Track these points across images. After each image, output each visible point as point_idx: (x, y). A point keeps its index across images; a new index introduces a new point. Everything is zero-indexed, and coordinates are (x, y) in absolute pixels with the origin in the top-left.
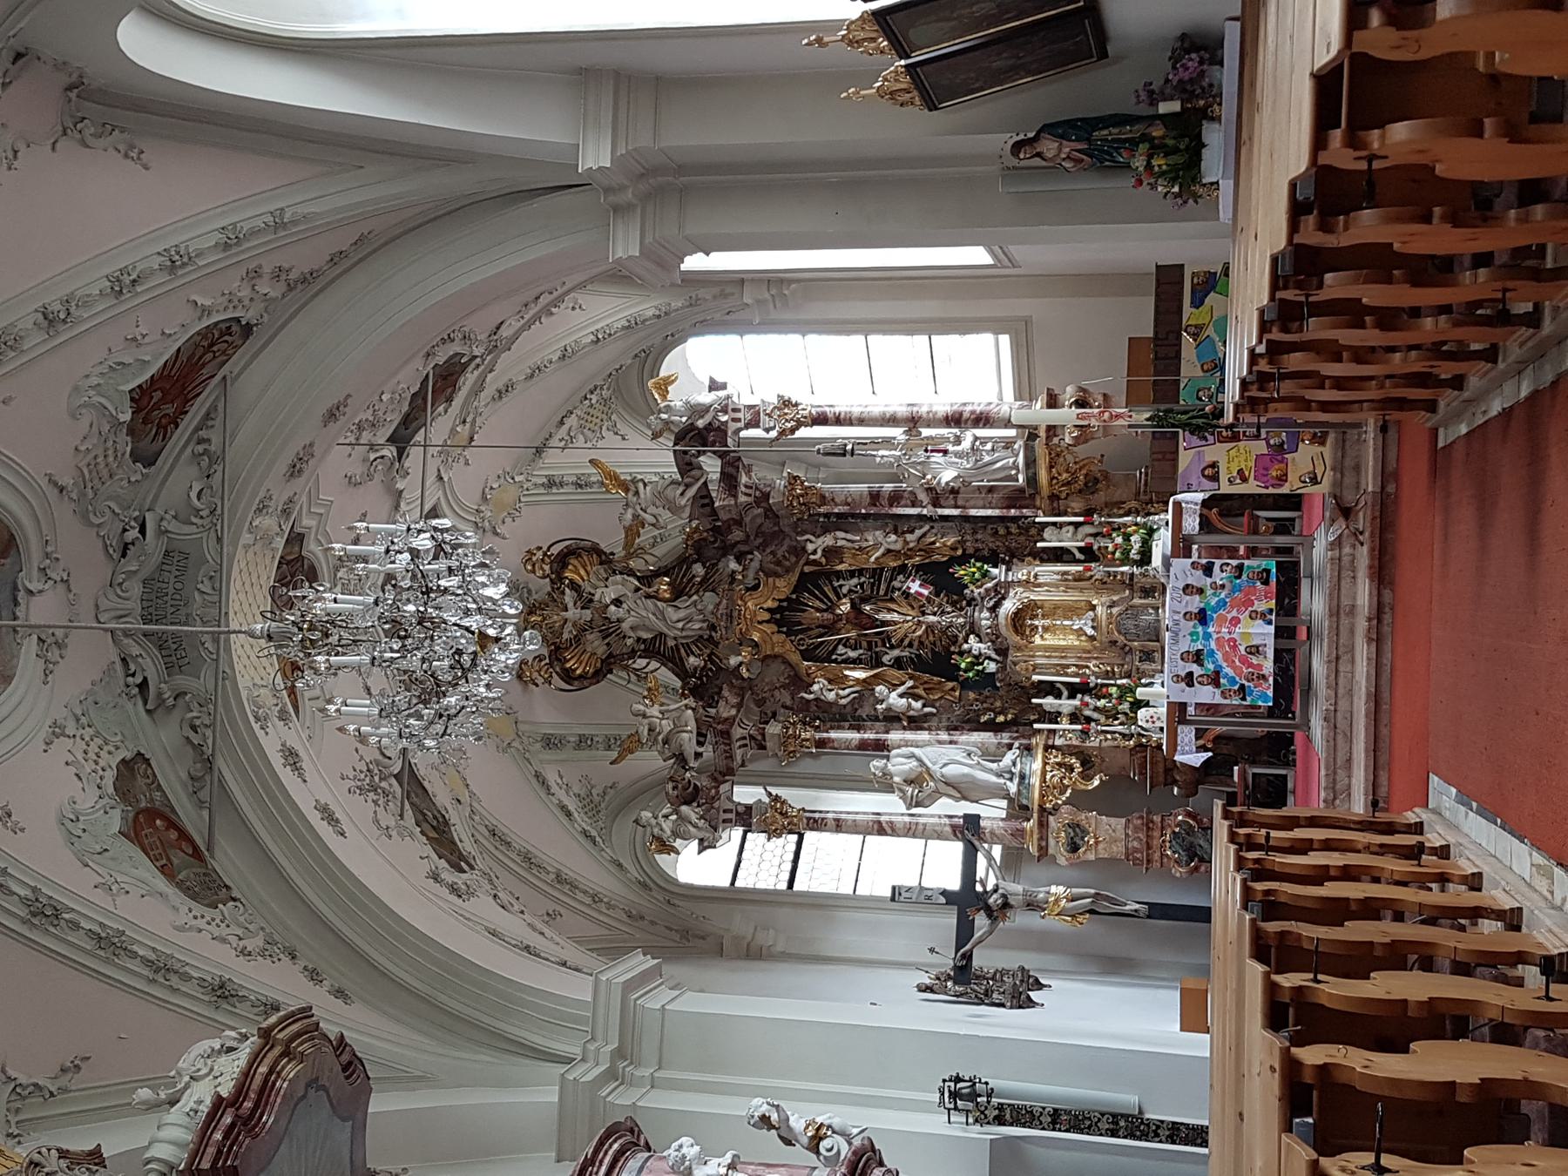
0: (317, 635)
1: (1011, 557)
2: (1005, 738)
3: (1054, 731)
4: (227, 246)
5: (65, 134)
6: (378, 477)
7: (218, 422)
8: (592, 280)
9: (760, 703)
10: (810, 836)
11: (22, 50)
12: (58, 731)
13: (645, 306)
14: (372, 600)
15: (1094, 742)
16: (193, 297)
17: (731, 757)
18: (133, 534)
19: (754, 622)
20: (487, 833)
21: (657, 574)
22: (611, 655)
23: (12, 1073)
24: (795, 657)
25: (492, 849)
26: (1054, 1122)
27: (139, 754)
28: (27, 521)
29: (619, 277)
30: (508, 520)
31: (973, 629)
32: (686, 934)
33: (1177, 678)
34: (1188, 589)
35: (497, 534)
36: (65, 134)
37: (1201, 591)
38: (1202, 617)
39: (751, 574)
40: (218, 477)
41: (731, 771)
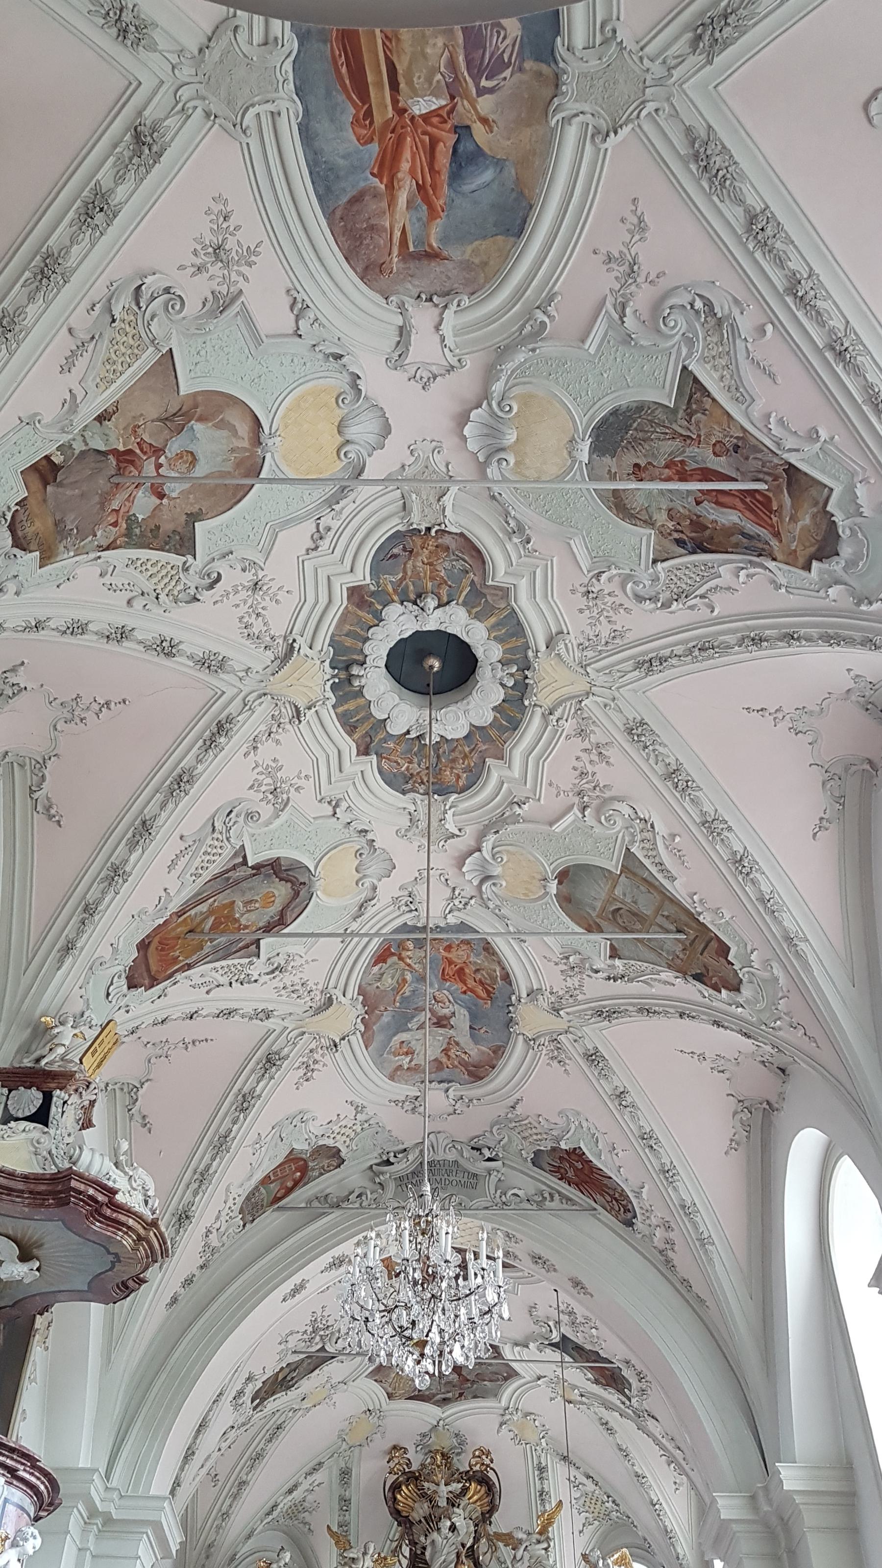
0: (423, 1225)
4: (683, 1207)
5: (739, 1101)
6: (536, 1328)
7: (565, 1206)
11: (787, 1073)
12: (359, 1109)
14: (448, 1258)
16: (646, 1186)
18: (487, 1154)
20: (279, 1422)
22: (412, 1524)
23: (146, 1084)
25: (267, 1428)
27: (344, 1161)
29: (703, 1509)
30: (511, 1435)
35: (501, 1426)
36: (739, 1101)
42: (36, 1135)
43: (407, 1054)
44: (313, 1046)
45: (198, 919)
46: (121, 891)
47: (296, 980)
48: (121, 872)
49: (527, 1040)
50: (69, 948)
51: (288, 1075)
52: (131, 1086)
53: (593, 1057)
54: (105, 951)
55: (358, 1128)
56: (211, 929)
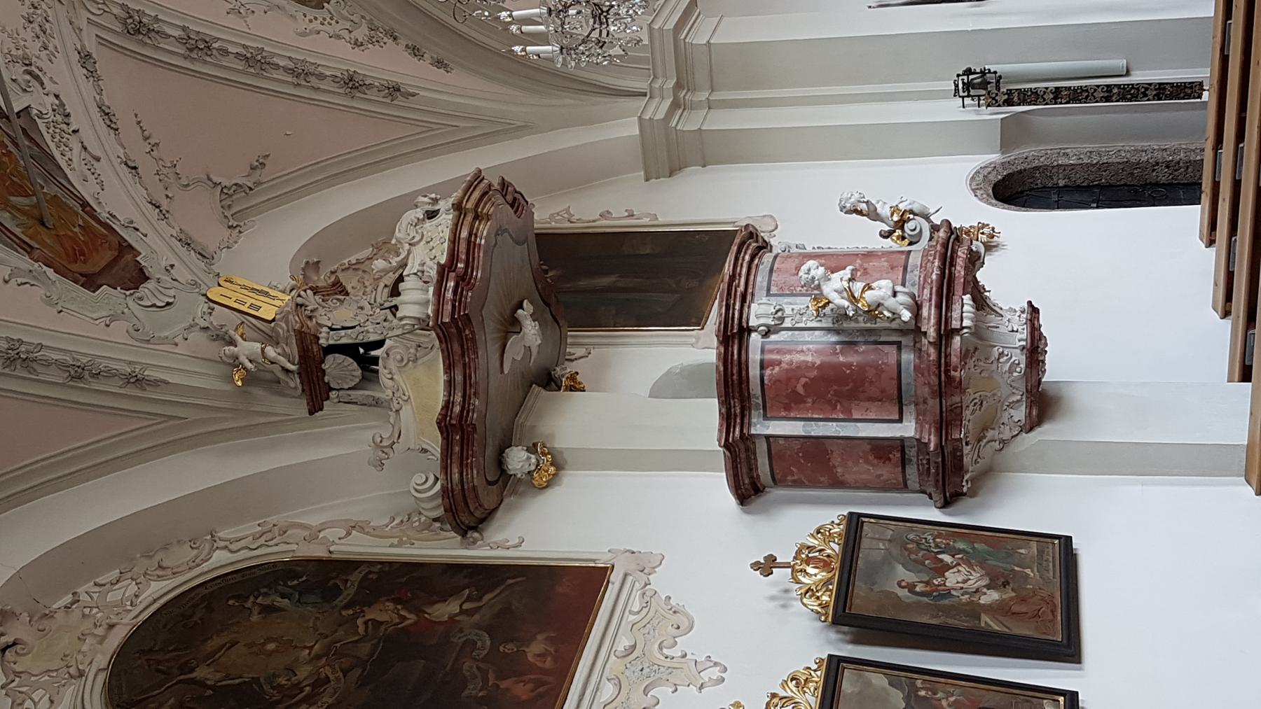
23: (216, 179)
26: (1055, 98)
42: (392, 365)
45: (24, 219)
46: (36, 342)
47: (29, 35)
48: (13, 353)
50: (137, 381)
52: (224, 197)
54: (119, 330)
56: (27, 196)
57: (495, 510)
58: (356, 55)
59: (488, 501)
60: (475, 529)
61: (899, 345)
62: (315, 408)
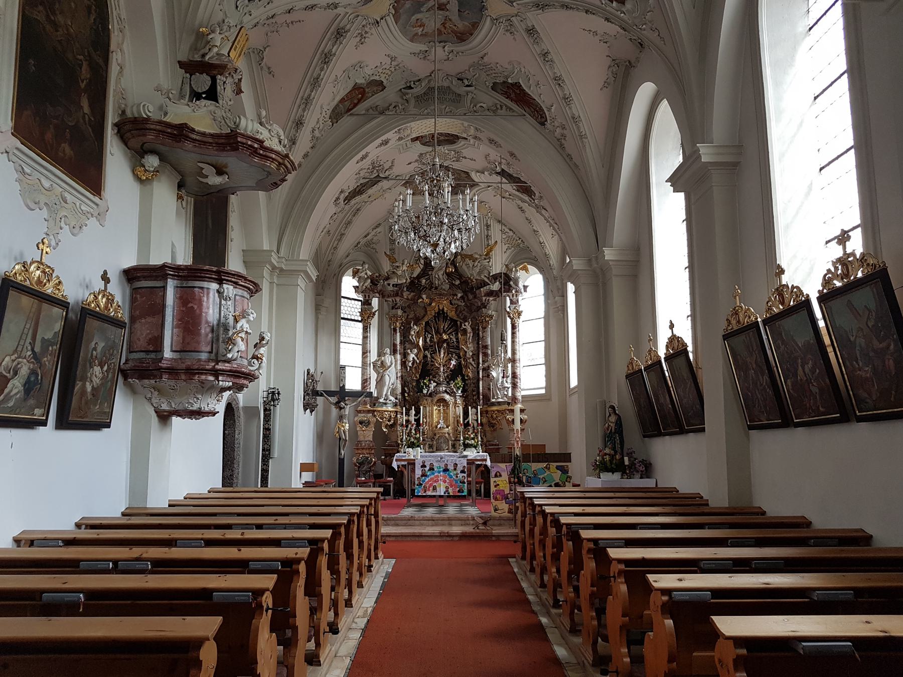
1: (465, 397)
2: (399, 397)
3: (402, 414)
4: (573, 118)
8: (563, 243)
9: (409, 306)
10: (360, 325)
13: (554, 261)
15: (399, 428)
17: (388, 297)
18: (466, 83)
19: (439, 303)
21: (455, 267)
24: (426, 319)
28: (471, 45)
31: (438, 384)
32: (324, 282)
33: (424, 462)
34: (456, 465)
37: (455, 469)
38: (446, 470)
39: (456, 302)
40: (488, 113)
41: (383, 297)
43: (420, 26)
44: (364, 23)
49: (492, 20)
51: (350, 41)
53: (531, 31)
55: (393, 69)
57: (126, 144)
58: (309, 129)
59: (133, 142)
60: (119, 132)
61: (211, 352)
62: (182, 64)
